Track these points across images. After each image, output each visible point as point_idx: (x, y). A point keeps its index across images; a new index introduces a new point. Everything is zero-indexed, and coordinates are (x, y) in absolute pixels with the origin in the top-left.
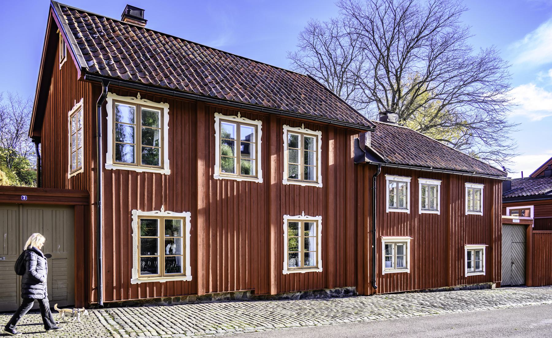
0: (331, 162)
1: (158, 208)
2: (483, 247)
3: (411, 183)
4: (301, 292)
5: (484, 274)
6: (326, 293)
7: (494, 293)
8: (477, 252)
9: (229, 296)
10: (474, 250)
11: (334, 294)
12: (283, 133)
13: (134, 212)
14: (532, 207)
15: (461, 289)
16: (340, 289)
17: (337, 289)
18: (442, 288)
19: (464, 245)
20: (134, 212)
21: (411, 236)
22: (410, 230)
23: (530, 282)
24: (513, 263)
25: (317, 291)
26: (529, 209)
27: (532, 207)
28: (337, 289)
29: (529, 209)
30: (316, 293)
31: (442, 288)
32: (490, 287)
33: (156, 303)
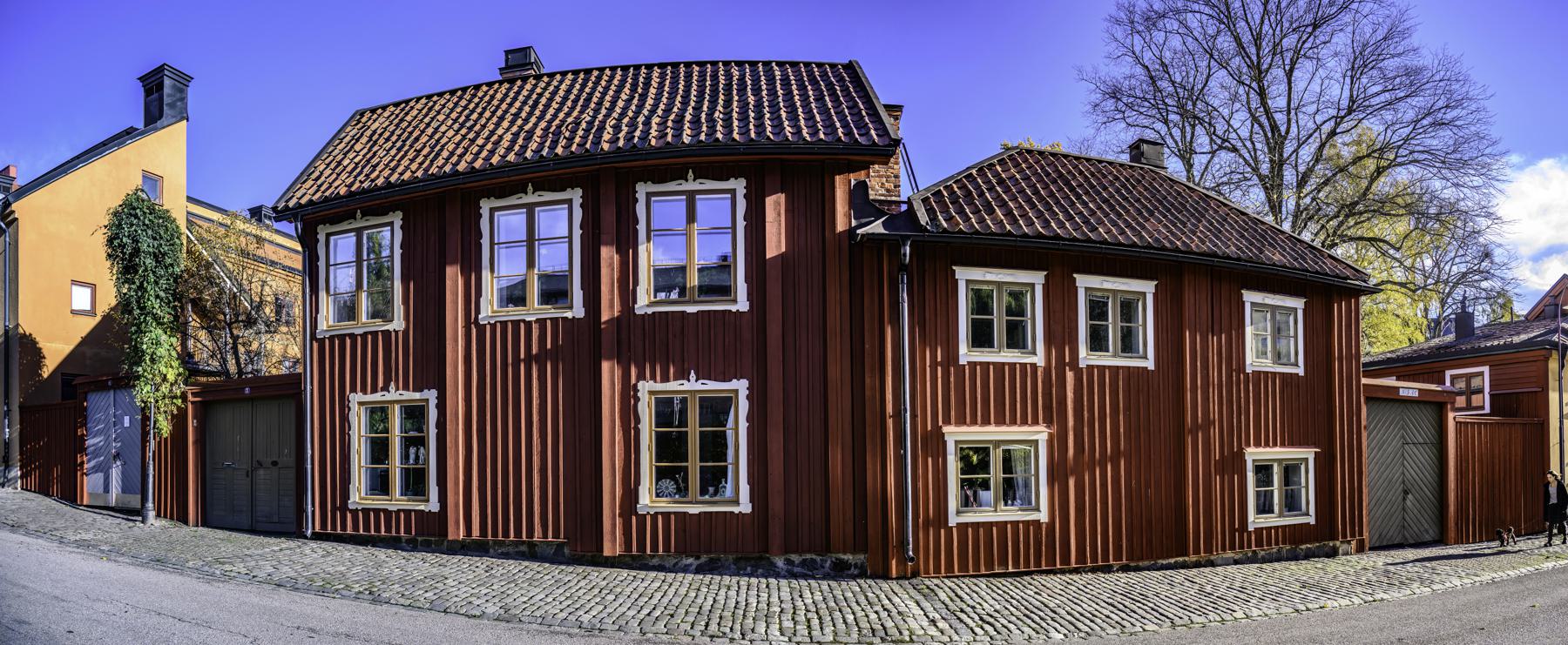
0: (775, 245)
1: (386, 388)
2: (1309, 453)
3: (1155, 295)
4: (698, 558)
5: (1312, 520)
6: (774, 565)
7: (1349, 566)
8: (1290, 471)
9: (523, 548)
10: (1279, 461)
11: (796, 570)
12: (636, 200)
13: (640, 385)
14: (1486, 369)
15: (1236, 562)
16: (818, 559)
17: (808, 556)
18: (1172, 561)
19: (1241, 450)
20: (640, 385)
21: (1048, 422)
22: (1048, 408)
23: (1452, 534)
24: (1406, 492)
25: (747, 559)
26: (1482, 374)
27: (1486, 369)
28: (808, 556)
29: (1482, 374)
30: (742, 564)
31: (1172, 561)
32: (1333, 553)
33: (393, 543)
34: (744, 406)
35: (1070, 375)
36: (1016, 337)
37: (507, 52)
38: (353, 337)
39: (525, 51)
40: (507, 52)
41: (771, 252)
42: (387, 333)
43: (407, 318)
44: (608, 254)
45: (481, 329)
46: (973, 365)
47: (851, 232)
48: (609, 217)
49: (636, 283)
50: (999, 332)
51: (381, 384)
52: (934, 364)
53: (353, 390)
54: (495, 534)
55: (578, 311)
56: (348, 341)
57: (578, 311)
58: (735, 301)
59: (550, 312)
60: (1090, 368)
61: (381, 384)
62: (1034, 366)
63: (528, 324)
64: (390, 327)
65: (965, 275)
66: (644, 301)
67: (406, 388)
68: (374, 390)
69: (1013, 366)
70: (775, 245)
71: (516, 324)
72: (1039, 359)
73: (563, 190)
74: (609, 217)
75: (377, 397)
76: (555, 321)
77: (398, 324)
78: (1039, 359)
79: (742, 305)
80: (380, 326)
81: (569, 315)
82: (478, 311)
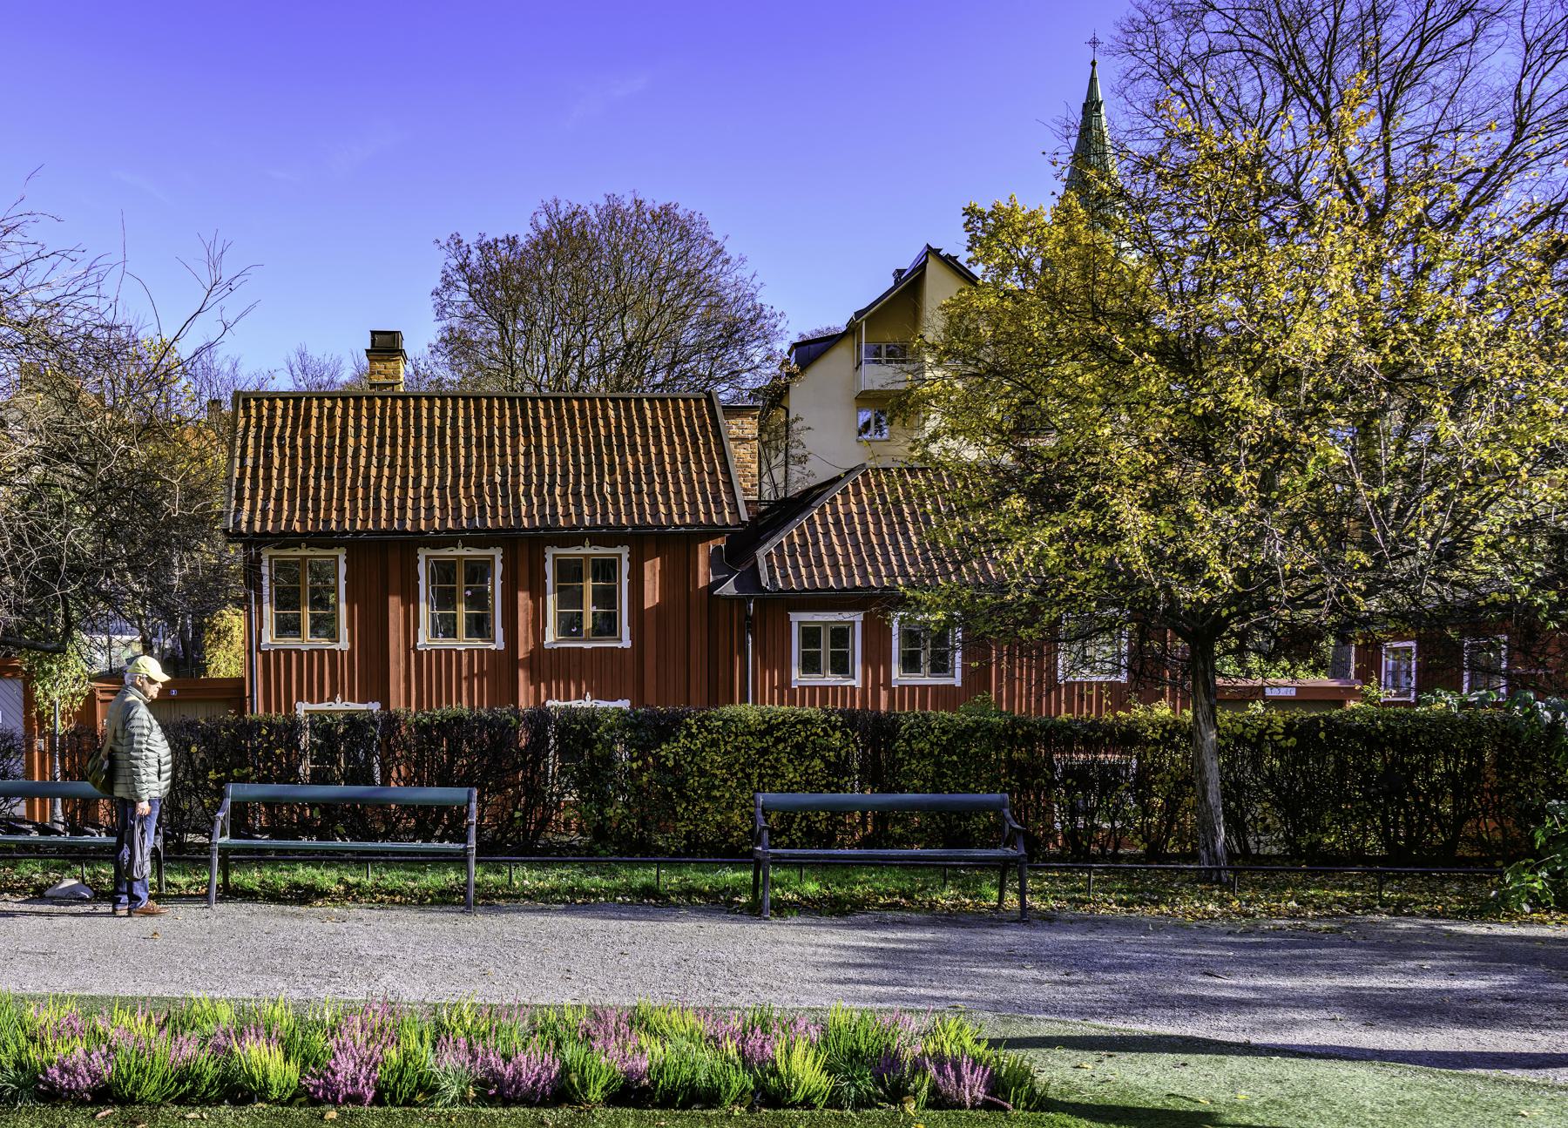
0: (651, 597)
1: (332, 699)
34: (499, 568)
35: (883, 694)
36: (841, 665)
37: (373, 333)
38: (299, 652)
39: (394, 336)
40: (373, 333)
41: (648, 604)
42: (333, 653)
43: (351, 639)
44: (523, 598)
45: (419, 655)
46: (803, 688)
47: (711, 587)
48: (523, 572)
49: (545, 624)
50: (826, 659)
51: (327, 695)
52: (772, 688)
53: (300, 699)
54: (912, 705)
55: (498, 644)
56: (294, 655)
57: (498, 644)
58: (620, 640)
59: (478, 643)
60: (902, 687)
61: (327, 695)
62: (853, 688)
63: (459, 653)
64: (336, 647)
65: (797, 618)
66: (551, 637)
67: (352, 699)
68: (321, 700)
69: (835, 688)
70: (651, 597)
71: (448, 652)
72: (857, 683)
73: (487, 547)
74: (523, 572)
75: (324, 706)
76: (481, 651)
77: (343, 644)
78: (857, 683)
79: (626, 643)
80: (324, 643)
81: (493, 647)
82: (416, 640)
